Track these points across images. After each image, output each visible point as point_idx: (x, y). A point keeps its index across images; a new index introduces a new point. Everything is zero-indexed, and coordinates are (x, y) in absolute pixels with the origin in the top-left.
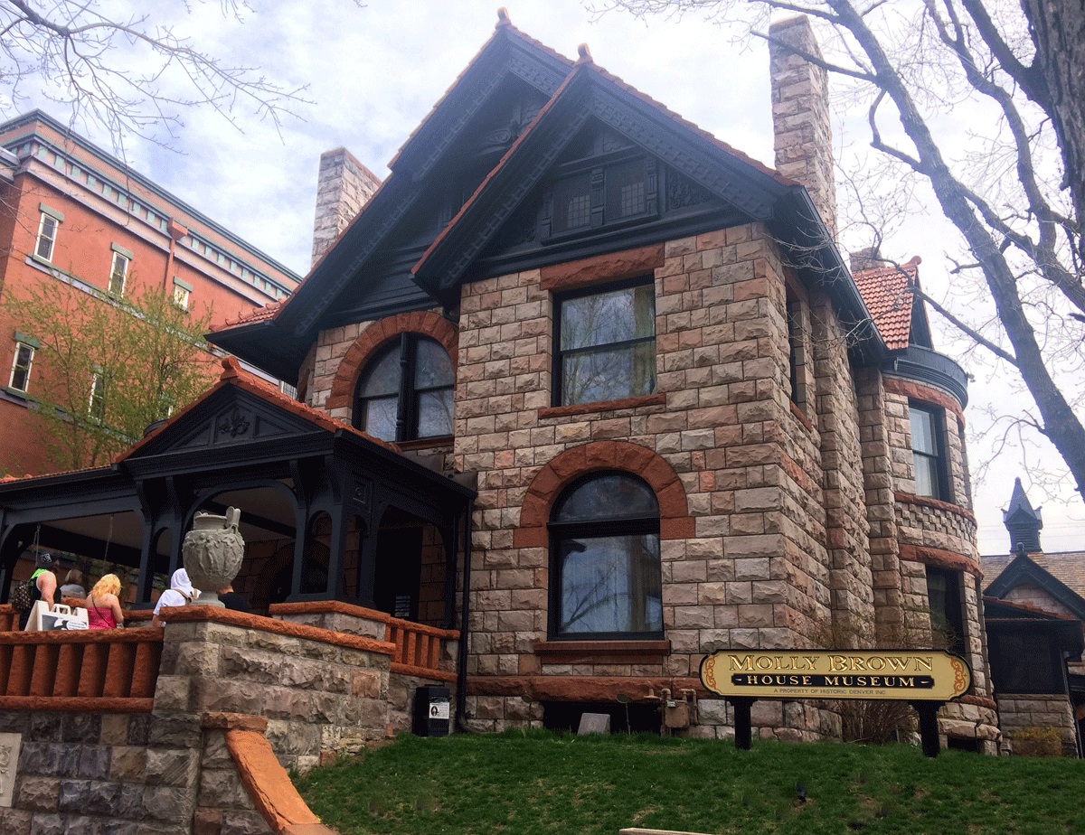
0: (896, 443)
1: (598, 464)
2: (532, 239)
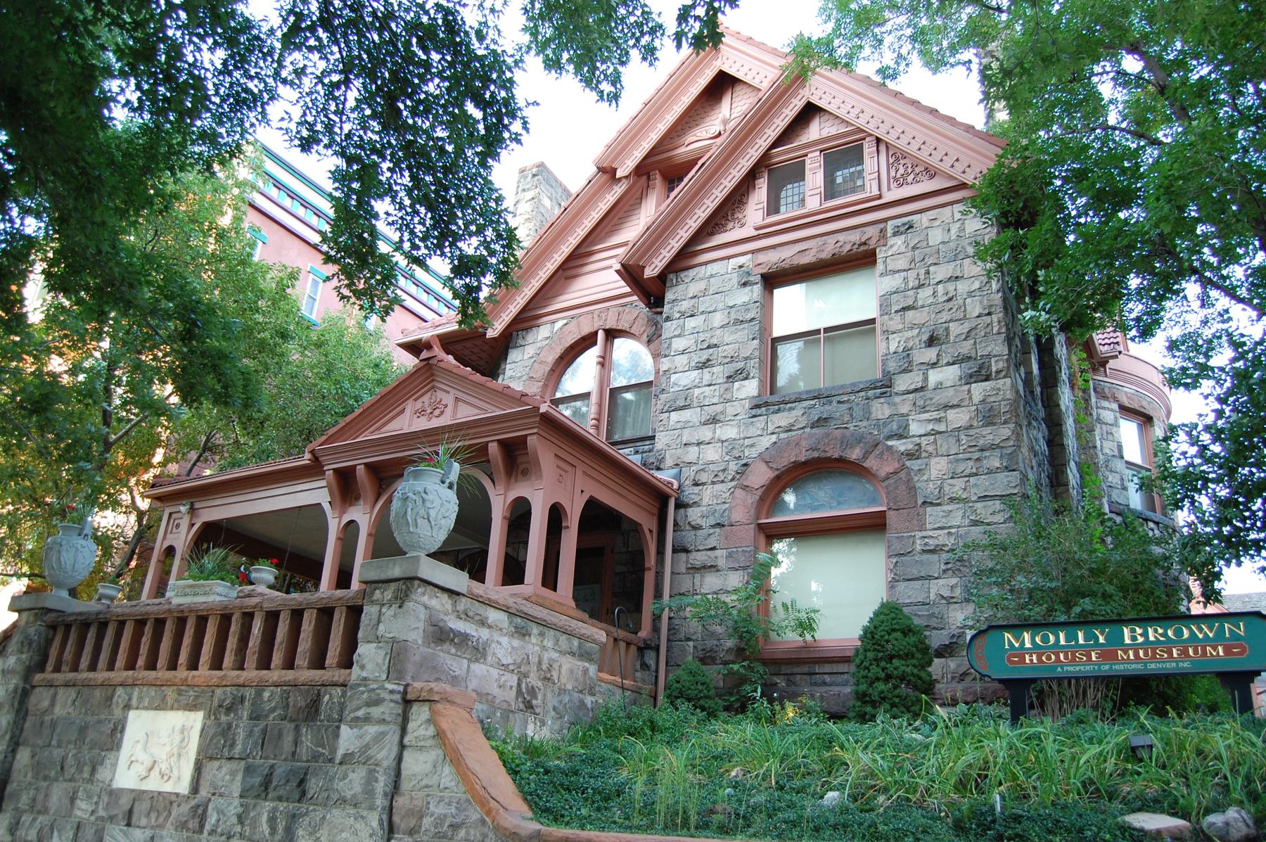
0: (1108, 451)
1: (816, 454)
2: (743, 225)
